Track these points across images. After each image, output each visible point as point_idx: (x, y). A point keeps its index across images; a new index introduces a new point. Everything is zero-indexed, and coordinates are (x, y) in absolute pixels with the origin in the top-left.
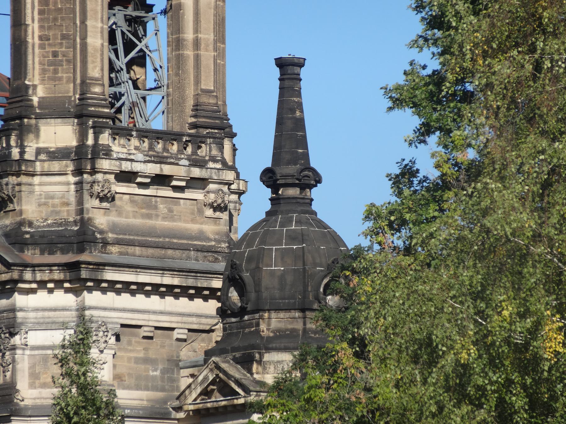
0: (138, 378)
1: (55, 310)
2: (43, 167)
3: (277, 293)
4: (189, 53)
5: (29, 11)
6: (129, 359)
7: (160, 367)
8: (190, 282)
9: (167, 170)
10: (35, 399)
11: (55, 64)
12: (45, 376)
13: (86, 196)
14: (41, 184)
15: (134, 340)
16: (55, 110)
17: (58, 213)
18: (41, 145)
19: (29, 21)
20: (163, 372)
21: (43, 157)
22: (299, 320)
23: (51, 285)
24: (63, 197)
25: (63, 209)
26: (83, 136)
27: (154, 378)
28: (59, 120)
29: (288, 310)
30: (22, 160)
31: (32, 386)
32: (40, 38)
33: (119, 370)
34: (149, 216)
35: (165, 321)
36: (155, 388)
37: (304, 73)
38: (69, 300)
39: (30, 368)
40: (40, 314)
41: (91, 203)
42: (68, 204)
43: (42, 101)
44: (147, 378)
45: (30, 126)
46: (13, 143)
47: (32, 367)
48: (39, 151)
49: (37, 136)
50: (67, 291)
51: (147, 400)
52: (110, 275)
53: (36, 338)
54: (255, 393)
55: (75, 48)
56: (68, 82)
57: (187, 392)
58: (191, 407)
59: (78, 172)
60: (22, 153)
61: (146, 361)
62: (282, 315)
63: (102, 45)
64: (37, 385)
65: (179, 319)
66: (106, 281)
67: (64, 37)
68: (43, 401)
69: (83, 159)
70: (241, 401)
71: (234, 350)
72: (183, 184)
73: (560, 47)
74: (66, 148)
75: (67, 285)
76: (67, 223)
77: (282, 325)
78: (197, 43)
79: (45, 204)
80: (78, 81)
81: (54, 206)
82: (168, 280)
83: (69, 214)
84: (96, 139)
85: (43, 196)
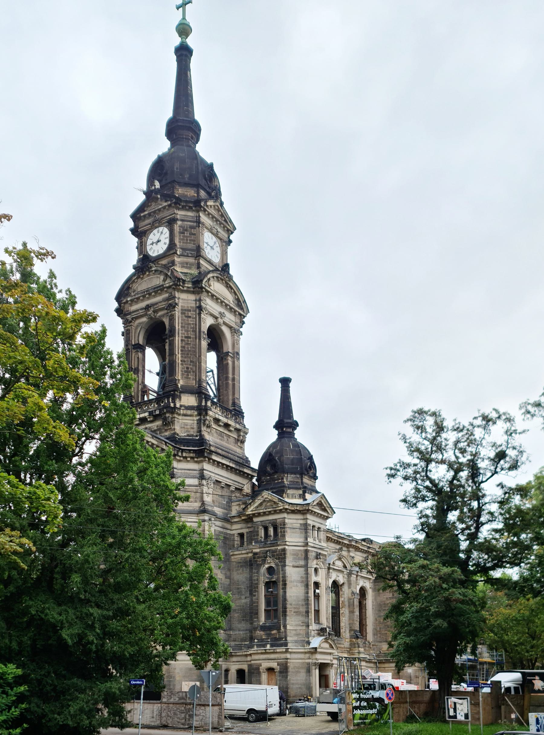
0: (219, 503)
5: (177, 349)
8: (238, 468)
9: (230, 422)
14: (182, 419)
17: (189, 431)
18: (182, 404)
19: (177, 353)
21: (183, 408)
26: (200, 402)
28: (190, 395)
29: (295, 474)
30: (175, 407)
32: (181, 361)
34: (221, 440)
35: (229, 482)
36: (224, 509)
37: (291, 385)
38: (196, 466)
40: (183, 471)
41: (204, 428)
42: (193, 428)
43: (182, 386)
45: (177, 395)
46: (171, 401)
48: (181, 406)
49: (180, 399)
50: (196, 462)
52: (214, 457)
55: (196, 367)
56: (193, 379)
58: (251, 513)
59: (199, 414)
60: (175, 405)
66: (212, 459)
67: (191, 362)
69: (202, 411)
70: (282, 508)
71: (271, 489)
72: (233, 429)
73: (52, 520)
75: (196, 459)
76: (192, 436)
77: (292, 480)
79: (184, 427)
82: (231, 465)
83: (194, 432)
84: (206, 403)
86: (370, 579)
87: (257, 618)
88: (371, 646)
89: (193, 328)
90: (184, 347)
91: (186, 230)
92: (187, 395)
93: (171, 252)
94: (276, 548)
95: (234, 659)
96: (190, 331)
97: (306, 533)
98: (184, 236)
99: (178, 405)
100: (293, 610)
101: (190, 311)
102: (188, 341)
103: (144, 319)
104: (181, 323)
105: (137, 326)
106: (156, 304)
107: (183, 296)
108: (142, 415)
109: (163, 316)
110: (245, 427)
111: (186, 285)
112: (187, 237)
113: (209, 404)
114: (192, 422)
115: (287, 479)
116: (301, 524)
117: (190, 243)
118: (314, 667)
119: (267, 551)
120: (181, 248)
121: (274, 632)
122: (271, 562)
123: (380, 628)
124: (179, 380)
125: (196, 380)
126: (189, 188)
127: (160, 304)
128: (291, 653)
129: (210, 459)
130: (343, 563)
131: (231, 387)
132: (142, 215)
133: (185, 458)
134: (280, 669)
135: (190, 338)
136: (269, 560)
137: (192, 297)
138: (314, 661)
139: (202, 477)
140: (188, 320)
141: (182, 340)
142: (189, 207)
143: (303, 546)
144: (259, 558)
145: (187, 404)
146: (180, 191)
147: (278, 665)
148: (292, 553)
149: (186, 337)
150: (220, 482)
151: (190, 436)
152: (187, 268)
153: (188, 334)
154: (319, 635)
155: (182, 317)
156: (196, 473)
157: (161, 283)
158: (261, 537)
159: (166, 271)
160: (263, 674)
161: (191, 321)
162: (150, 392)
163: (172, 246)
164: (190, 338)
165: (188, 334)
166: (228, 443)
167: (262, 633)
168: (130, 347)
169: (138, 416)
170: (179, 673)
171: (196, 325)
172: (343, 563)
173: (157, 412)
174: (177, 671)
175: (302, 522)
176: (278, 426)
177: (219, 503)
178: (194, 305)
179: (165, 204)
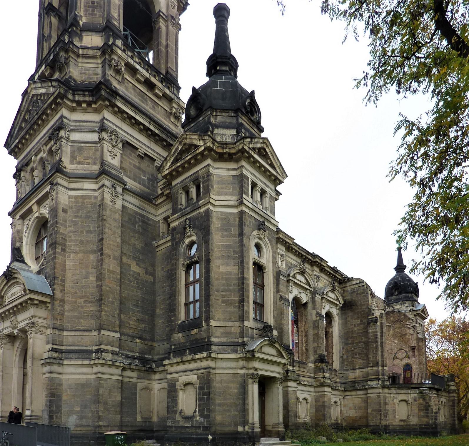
0: (135, 175)
2: (83, 52)
4: (163, 49)
6: (130, 163)
7: (147, 176)
10: (73, 170)
12: (80, 158)
13: (107, 67)
14: (82, 63)
15: (133, 154)
22: (234, 118)
24: (94, 70)
25: (94, 76)
27: (143, 180)
31: (72, 163)
33: (123, 165)
35: (150, 153)
36: (143, 185)
38: (96, 118)
39: (70, 153)
40: (78, 124)
42: (97, 74)
43: (84, 23)
44: (140, 178)
47: (72, 153)
49: (81, 39)
51: (140, 190)
53: (76, 136)
54: (231, 288)
57: (164, 164)
59: (104, 53)
61: (139, 168)
63: (120, 5)
64: (75, 162)
65: (158, 156)
68: (78, 171)
70: (203, 148)
77: (222, 120)
78: (167, 46)
79: (85, 73)
80: (105, 16)
81: (89, 74)
85: (83, 69)
86: (337, 305)
87: (175, 315)
88: (338, 374)
92: (90, 34)
94: (197, 212)
95: (157, 377)
97: (241, 187)
114: (95, 66)
116: (233, 176)
118: (250, 381)
121: (195, 331)
123: (347, 356)
124: (81, 17)
125: (103, 17)
128: (215, 359)
129: (113, 105)
130: (306, 279)
131: (164, 54)
133: (79, 103)
134: (200, 383)
136: (189, 232)
138: (251, 371)
139: (102, 129)
143: (237, 206)
144: (178, 233)
147: (198, 378)
150: (137, 149)
154: (261, 336)
156: (96, 128)
158: (181, 205)
160: (181, 392)
162: (191, 317)
166: (155, 111)
167: (180, 335)
170: (66, 391)
172: (306, 279)
174: (64, 387)
175: (235, 173)
177: (135, 175)
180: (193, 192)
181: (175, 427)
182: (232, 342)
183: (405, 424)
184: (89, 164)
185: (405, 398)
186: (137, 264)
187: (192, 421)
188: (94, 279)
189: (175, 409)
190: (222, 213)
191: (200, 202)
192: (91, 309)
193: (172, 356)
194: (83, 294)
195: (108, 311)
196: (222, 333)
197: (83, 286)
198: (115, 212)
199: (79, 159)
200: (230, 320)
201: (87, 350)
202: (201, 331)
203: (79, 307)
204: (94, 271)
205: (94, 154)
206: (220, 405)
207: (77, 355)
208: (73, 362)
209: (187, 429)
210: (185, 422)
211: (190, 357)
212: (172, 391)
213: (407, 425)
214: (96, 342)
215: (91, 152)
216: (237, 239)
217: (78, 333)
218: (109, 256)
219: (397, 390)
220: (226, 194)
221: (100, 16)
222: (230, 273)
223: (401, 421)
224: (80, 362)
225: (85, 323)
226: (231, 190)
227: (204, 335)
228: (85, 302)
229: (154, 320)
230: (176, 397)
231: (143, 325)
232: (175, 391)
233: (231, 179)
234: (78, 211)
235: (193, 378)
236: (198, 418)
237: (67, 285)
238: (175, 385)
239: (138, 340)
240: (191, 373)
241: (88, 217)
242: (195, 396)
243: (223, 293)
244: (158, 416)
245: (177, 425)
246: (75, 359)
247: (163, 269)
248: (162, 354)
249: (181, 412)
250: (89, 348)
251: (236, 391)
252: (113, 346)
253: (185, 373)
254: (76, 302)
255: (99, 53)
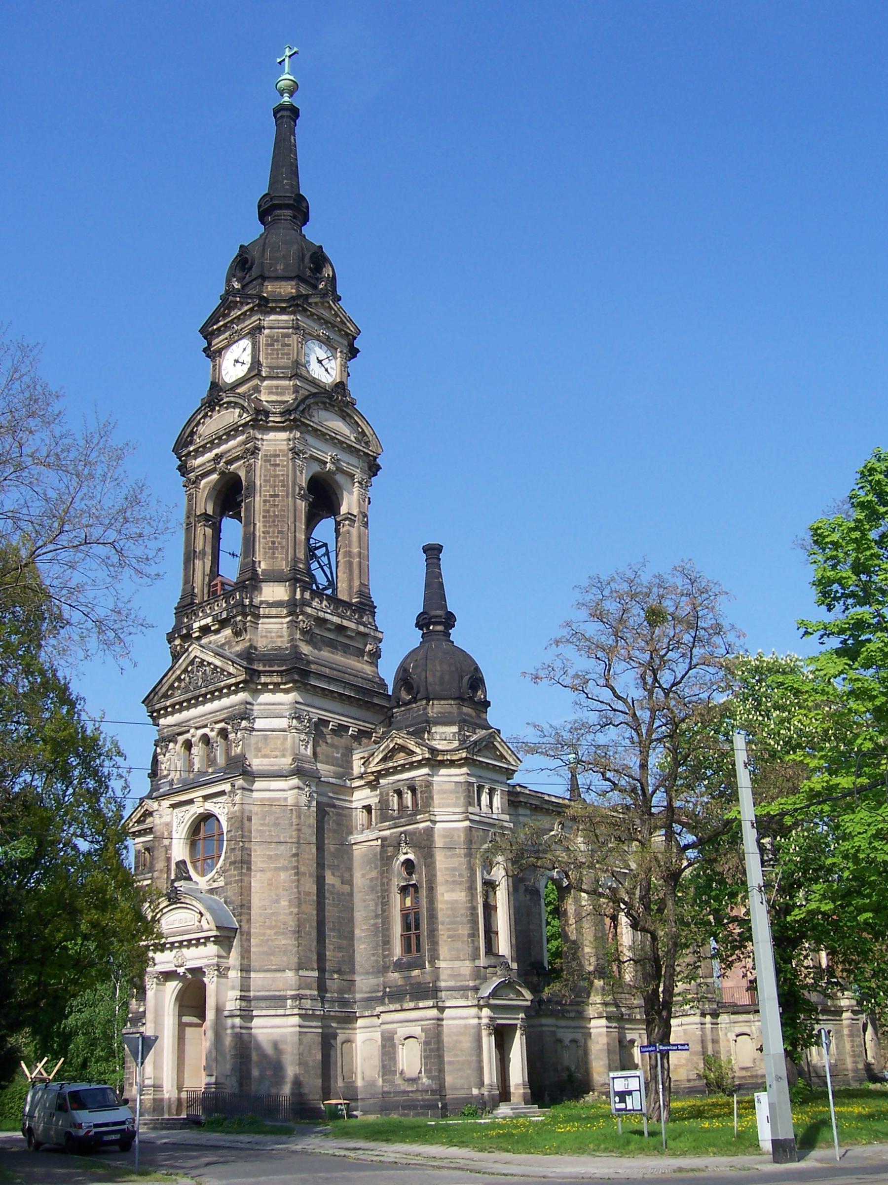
0: (327, 756)
1: (273, 704)
3: (437, 688)
7: (341, 751)
9: (345, 623)
11: (273, 548)
16: (275, 577)
20: (343, 755)
21: (264, 606)
23: (271, 687)
44: (333, 757)
48: (262, 602)
49: (261, 593)
54: (458, 919)
62: (442, 702)
67: (279, 532)
70: (420, 758)
72: (353, 635)
74: (280, 601)
79: (266, 637)
84: (302, 595)
87: (389, 949)
89: (283, 481)
90: (268, 511)
91: (277, 341)
93: (252, 374)
96: (278, 486)
98: (272, 350)
99: (256, 601)
100: (447, 933)
101: (278, 456)
102: (274, 501)
103: (215, 476)
104: (265, 476)
105: (205, 487)
106: (229, 451)
107: (272, 435)
108: (203, 622)
109: (239, 467)
110: (376, 630)
111: (271, 419)
112: (278, 350)
113: (307, 595)
114: (279, 626)
115: (433, 709)
117: (282, 358)
119: (401, 833)
120: (268, 367)
121: (416, 972)
122: (408, 854)
126: (283, 283)
127: (234, 451)
132: (215, 327)
135: (278, 496)
137: (284, 435)
140: (275, 471)
141: (265, 501)
142: (281, 308)
145: (271, 599)
146: (270, 289)
147: (422, 1030)
148: (442, 833)
149: (271, 496)
151: (276, 650)
152: (277, 394)
153: (274, 491)
155: (266, 466)
157: (236, 420)
159: (241, 402)
161: (279, 471)
163: (256, 363)
164: (278, 496)
165: (274, 491)
168: (192, 520)
169: (196, 625)
171: (288, 476)
173: (224, 615)
176: (423, 622)
177: (327, 756)
178: (285, 448)
179: (246, 308)
180: (408, 797)
181: (395, 1092)
182: (462, 986)
183: (749, 1074)
184: (276, 757)
185: (746, 1030)
186: (333, 874)
187: (417, 1084)
188: (286, 903)
189: (393, 1069)
190: (444, 829)
191: (418, 817)
192: (283, 942)
193: (387, 1001)
194: (274, 923)
195: (305, 945)
196: (450, 975)
197: (272, 914)
198: (310, 816)
199: (264, 751)
200: (458, 959)
201: (280, 996)
202: (424, 973)
203: (268, 940)
204: (286, 893)
205: (283, 743)
206: (450, 1063)
207: (268, 1003)
208: (264, 1013)
209: (410, 1094)
210: (408, 1086)
211: (412, 1005)
212: (388, 1046)
213: (751, 1077)
214: (291, 985)
215: (279, 742)
216: (463, 860)
217: (268, 975)
218: (305, 874)
219: (732, 1016)
220: (448, 806)
221: (282, 559)
222: (456, 901)
223: (742, 1069)
224: (273, 1012)
225: (277, 960)
226: (454, 801)
227: (428, 978)
228: (276, 934)
229: (353, 945)
230: (394, 1053)
231: (341, 954)
232: (393, 1046)
233: (453, 786)
234: (264, 818)
235: (416, 1030)
236: (425, 1080)
237: (253, 912)
238: (391, 1039)
239: (336, 976)
240: (414, 1023)
241: (276, 825)
242: (419, 1053)
243: (448, 926)
244: (363, 1078)
245: (398, 1089)
246: (267, 1008)
247: (363, 876)
248: (366, 992)
249: (402, 1073)
250: (282, 993)
251: (469, 1045)
252: (311, 989)
253: (406, 1024)
254: (264, 934)
255: (285, 611)
